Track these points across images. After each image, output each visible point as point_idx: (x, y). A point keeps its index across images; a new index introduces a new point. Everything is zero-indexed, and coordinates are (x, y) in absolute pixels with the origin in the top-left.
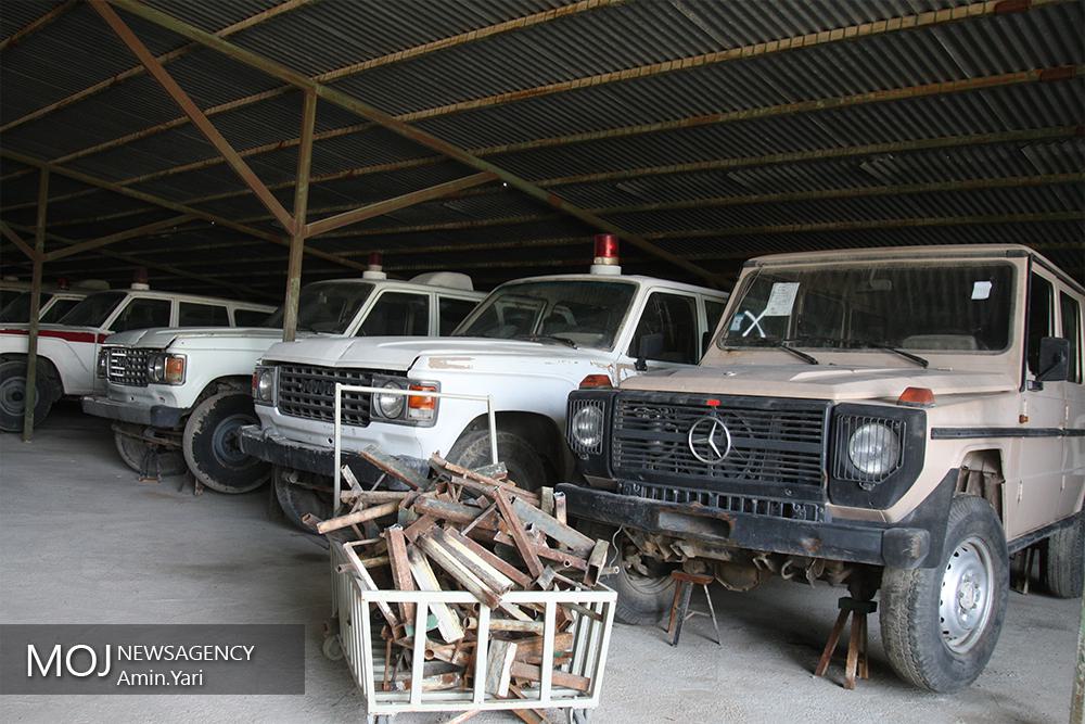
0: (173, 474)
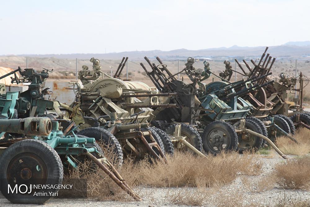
0: (19, 121)
